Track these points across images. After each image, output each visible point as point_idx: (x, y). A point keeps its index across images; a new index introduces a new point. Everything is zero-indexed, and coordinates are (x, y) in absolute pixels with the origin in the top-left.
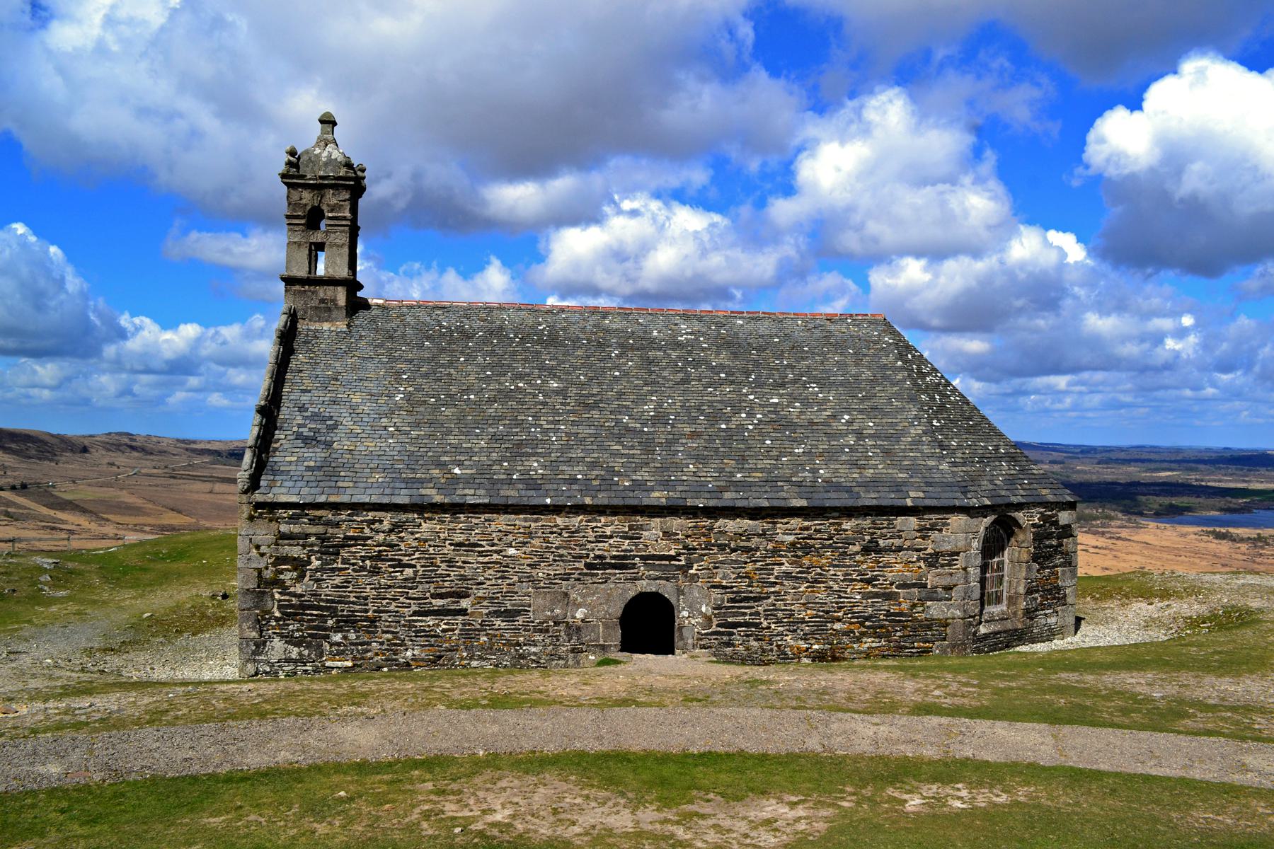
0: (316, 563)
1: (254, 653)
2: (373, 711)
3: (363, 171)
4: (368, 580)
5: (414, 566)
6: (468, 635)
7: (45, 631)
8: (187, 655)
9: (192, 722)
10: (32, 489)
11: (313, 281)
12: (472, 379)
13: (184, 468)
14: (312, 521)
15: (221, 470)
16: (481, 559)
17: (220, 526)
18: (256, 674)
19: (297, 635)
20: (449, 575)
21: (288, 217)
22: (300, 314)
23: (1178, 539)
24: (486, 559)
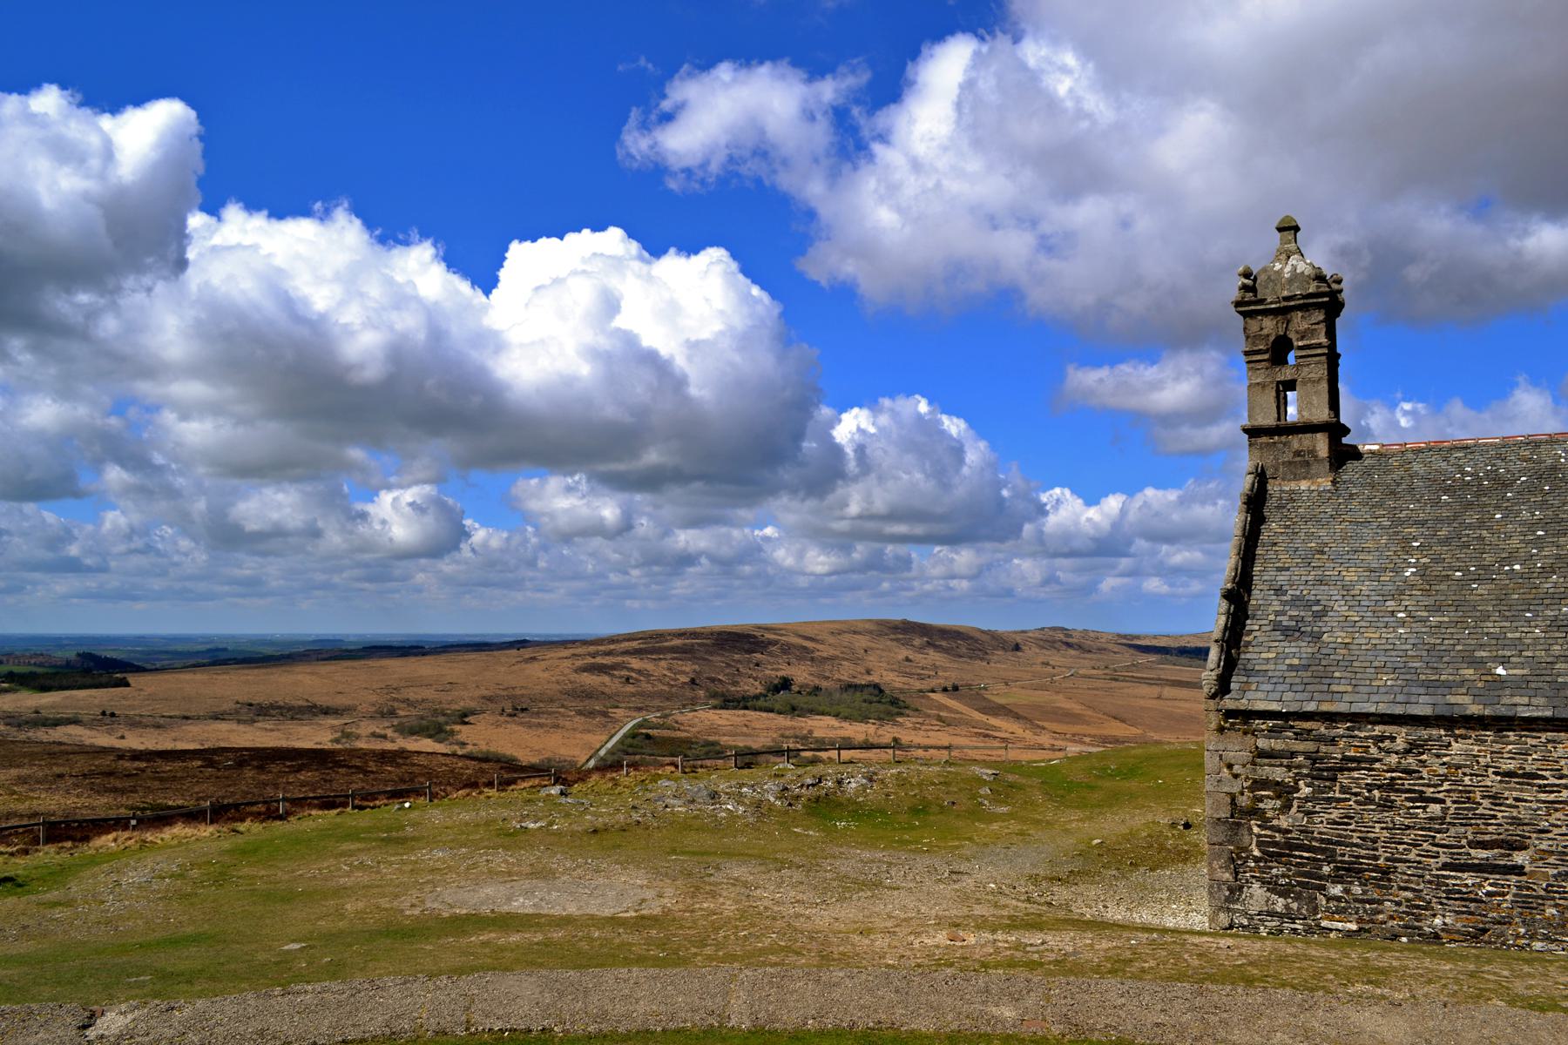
0: (1306, 791)
1: (1227, 900)
2: (1398, 996)
3: (1339, 282)
4: (1377, 817)
5: (1442, 801)
6: (1527, 903)
7: (987, 851)
8: (1143, 895)
9: (1162, 978)
10: (963, 690)
11: (1285, 430)
12: (1515, 542)
13: (1127, 668)
14: (1298, 736)
15: (1183, 671)
16: (1543, 796)
17: (1173, 740)
18: (1231, 927)
19: (1282, 881)
20: (1494, 817)
21: (1246, 353)
22: (1269, 473)
23: (786, 671)
24: (1552, 797)
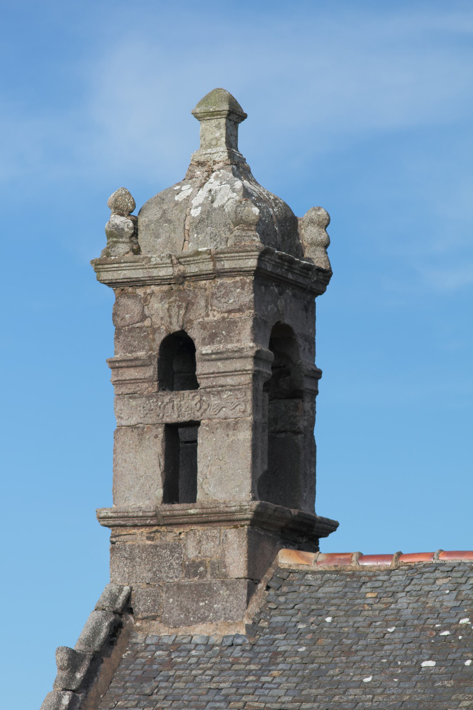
21: (115, 365)
22: (140, 606)
